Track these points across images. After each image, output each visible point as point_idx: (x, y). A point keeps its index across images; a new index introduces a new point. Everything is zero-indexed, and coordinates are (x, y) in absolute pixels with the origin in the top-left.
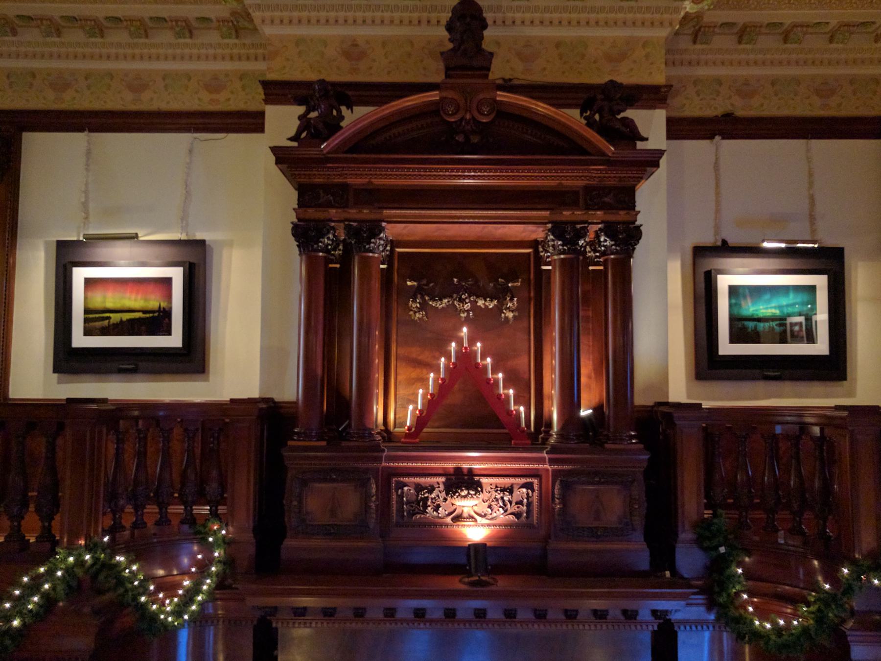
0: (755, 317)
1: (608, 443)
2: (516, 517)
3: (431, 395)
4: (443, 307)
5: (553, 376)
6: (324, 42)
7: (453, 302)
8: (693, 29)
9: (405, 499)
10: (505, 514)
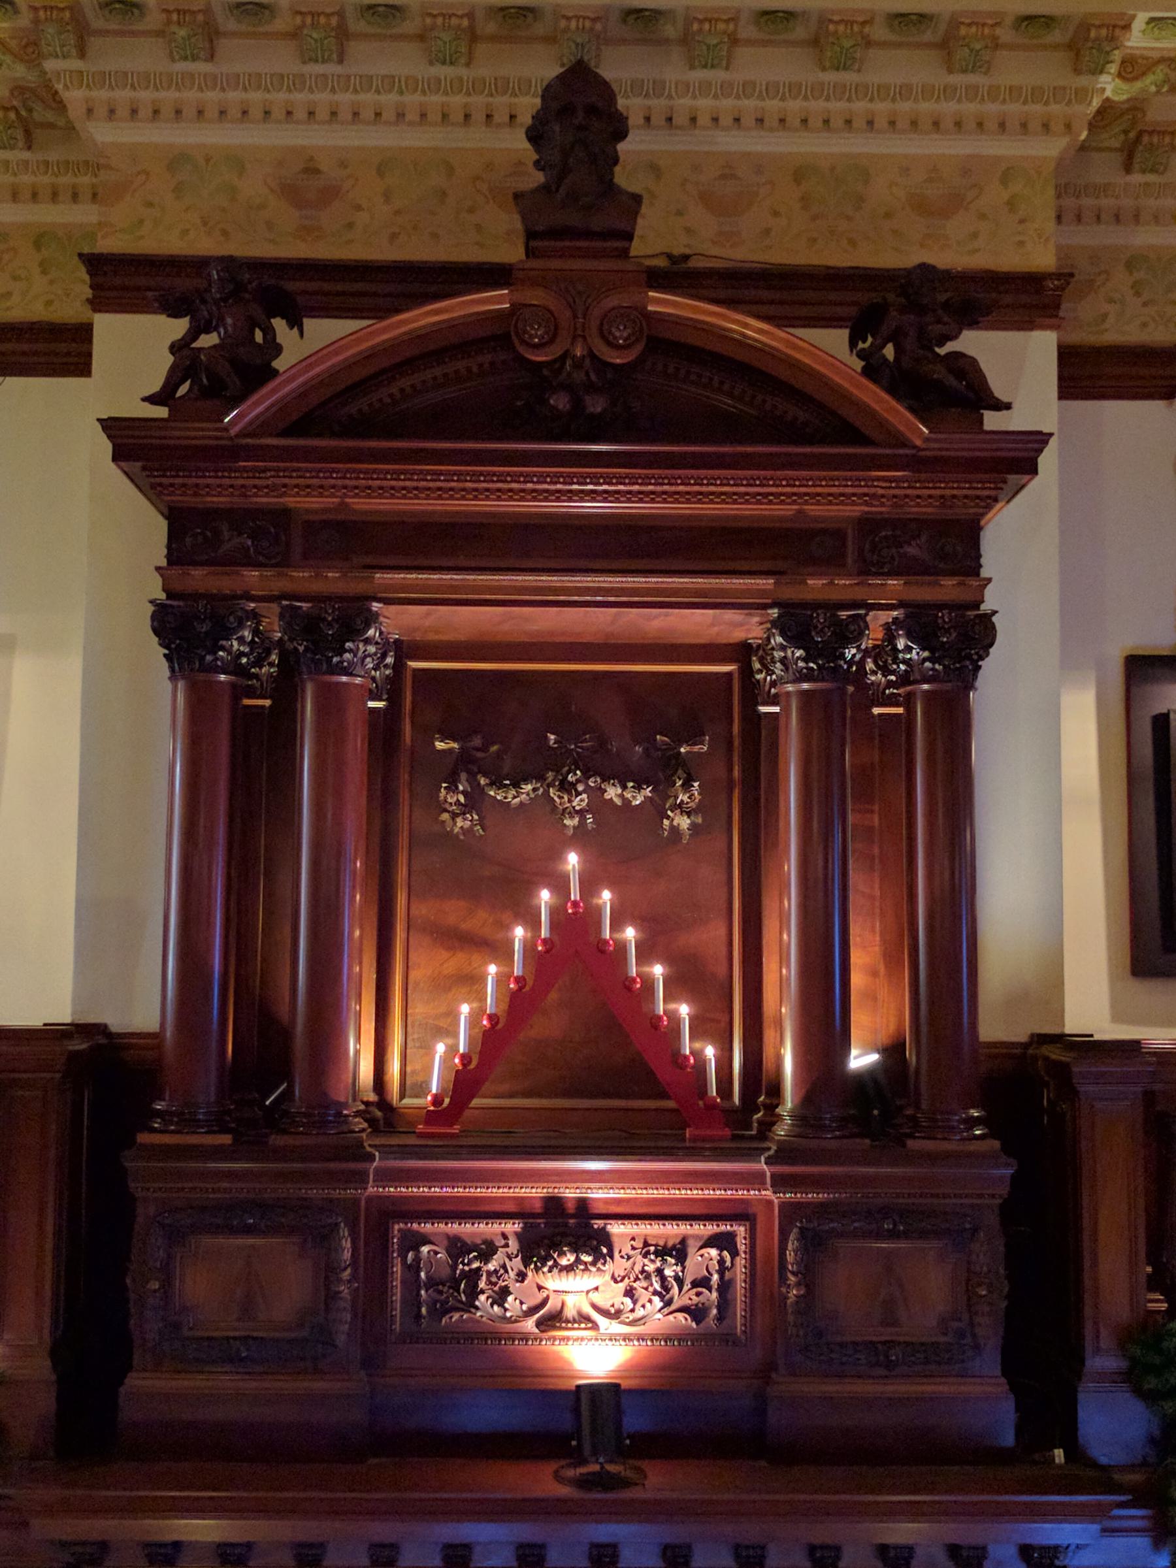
1: (915, 1138)
3: (490, 1017)
5: (784, 971)
6: (237, 161)
7: (546, 792)
8: (1122, 137)
9: (423, 1274)
10: (666, 1311)
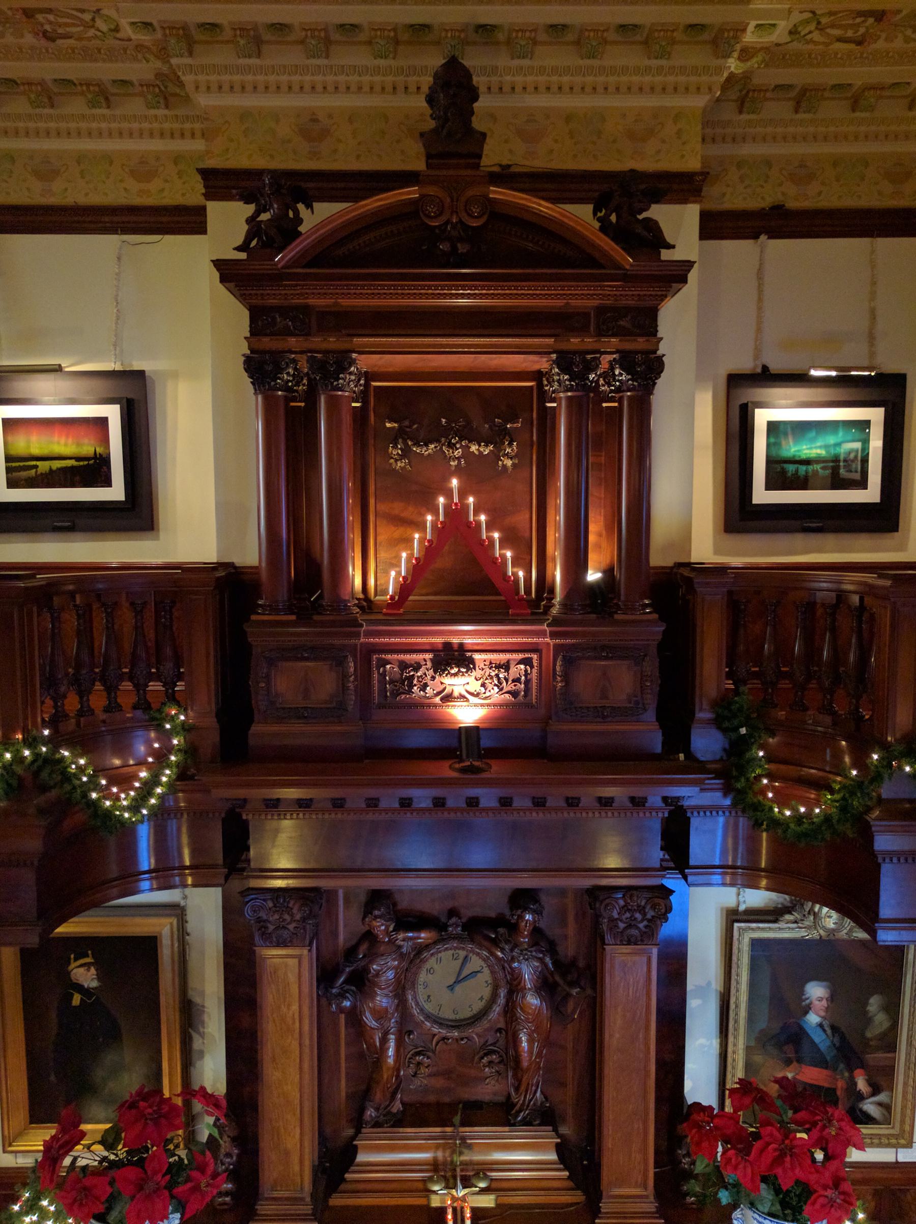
0: (797, 458)
2: (513, 697)
3: (416, 559)
4: (429, 454)
7: (441, 448)
9: (387, 678)
10: (500, 693)
